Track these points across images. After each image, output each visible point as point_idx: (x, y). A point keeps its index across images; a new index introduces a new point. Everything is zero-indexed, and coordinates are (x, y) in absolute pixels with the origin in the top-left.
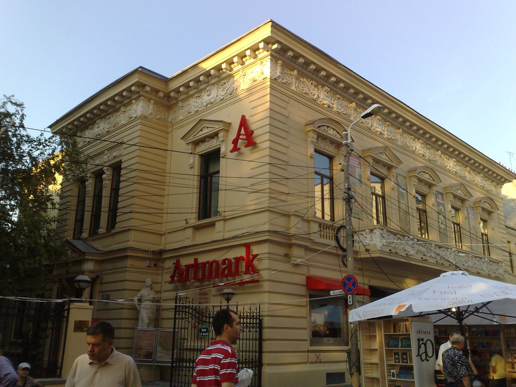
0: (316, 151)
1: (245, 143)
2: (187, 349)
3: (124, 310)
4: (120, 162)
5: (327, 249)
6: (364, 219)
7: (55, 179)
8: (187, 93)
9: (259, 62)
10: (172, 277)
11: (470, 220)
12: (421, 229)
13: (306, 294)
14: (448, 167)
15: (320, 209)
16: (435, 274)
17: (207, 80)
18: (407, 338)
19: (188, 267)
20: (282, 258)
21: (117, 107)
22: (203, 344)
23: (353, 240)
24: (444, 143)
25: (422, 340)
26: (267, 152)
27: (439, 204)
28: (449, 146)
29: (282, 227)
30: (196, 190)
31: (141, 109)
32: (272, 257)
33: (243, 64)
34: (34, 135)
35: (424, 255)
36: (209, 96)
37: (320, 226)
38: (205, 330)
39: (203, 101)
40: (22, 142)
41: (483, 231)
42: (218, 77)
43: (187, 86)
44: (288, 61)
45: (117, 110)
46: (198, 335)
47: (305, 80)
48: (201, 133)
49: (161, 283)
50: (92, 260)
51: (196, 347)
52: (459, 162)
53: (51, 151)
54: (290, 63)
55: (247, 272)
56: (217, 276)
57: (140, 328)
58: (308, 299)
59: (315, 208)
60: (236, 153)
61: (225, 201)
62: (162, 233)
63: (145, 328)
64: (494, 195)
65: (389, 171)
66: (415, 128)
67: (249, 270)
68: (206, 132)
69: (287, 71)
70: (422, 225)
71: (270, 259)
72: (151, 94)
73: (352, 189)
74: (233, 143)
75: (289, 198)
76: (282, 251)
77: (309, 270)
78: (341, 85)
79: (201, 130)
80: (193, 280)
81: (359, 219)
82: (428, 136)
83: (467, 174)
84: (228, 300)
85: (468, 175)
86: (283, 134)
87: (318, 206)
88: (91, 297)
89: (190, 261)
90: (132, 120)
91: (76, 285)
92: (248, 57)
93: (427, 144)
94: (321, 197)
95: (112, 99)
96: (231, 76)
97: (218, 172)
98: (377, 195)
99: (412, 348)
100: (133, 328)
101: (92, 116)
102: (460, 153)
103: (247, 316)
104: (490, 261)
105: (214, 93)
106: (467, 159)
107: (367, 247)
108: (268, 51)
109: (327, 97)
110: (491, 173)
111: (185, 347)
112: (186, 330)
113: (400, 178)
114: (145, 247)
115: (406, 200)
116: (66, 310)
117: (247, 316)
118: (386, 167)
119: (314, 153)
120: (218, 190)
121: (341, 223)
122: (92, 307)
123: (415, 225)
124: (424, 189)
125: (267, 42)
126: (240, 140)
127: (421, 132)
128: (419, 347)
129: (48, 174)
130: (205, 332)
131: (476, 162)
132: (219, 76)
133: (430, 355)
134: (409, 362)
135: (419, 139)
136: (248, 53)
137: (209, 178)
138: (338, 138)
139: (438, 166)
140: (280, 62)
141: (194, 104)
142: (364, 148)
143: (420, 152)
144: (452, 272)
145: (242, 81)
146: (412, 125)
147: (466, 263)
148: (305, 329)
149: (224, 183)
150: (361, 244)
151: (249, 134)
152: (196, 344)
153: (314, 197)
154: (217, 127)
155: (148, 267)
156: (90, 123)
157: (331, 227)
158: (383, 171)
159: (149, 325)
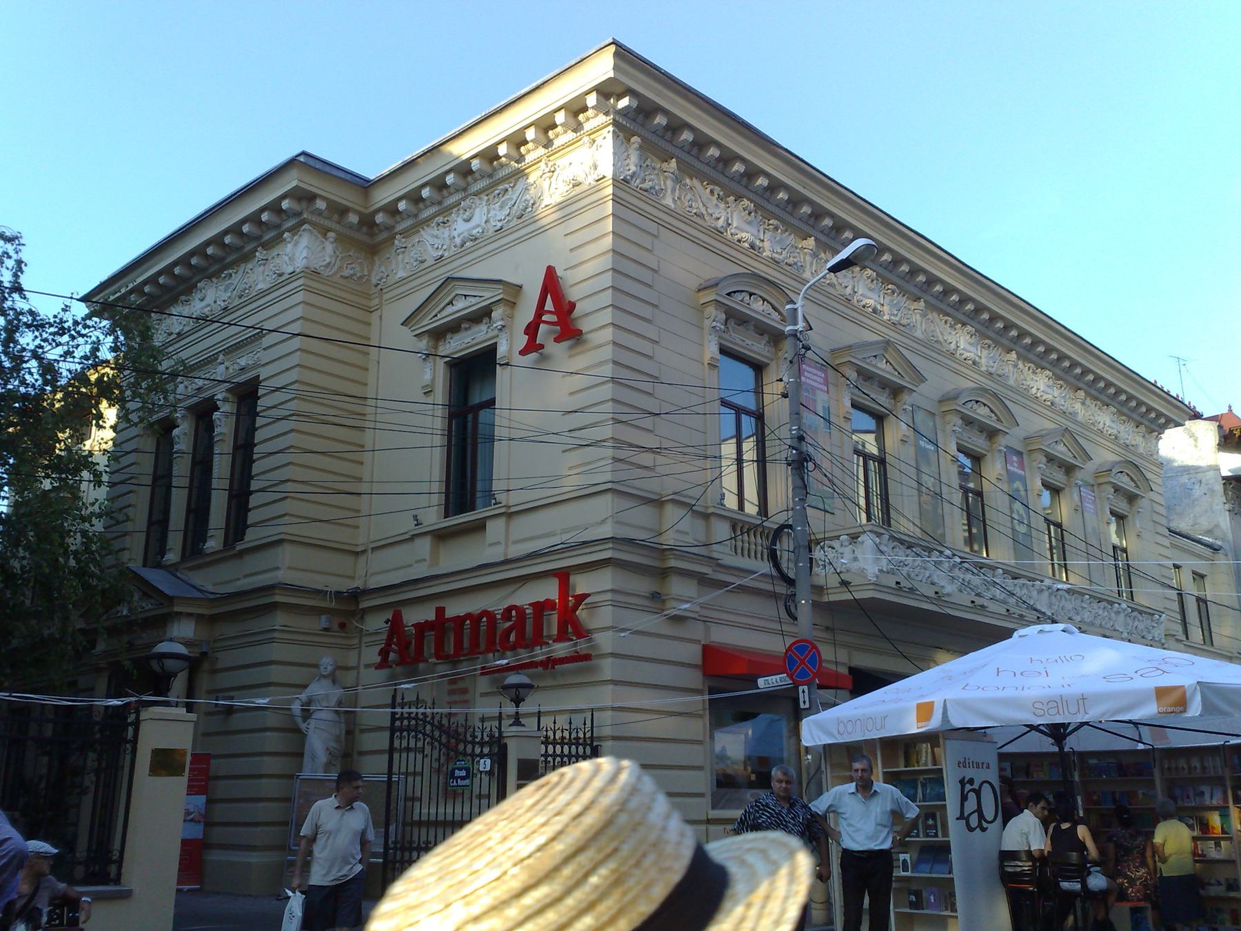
0: (724, 351)
1: (553, 332)
2: (420, 823)
3: (268, 734)
4: (255, 383)
5: (746, 581)
6: (836, 511)
7: (100, 416)
8: (416, 216)
9: (586, 139)
10: (384, 653)
11: (1086, 514)
12: (970, 540)
13: (700, 687)
14: (1034, 390)
15: (734, 484)
16: (1006, 634)
17: (462, 183)
18: (937, 778)
19: (421, 627)
20: (647, 603)
21: (248, 248)
22: (458, 810)
23: (811, 559)
24: (1023, 333)
25: (971, 781)
26: (607, 352)
27: (1012, 477)
28: (1037, 342)
29: (645, 529)
30: (439, 440)
31: (304, 255)
32: (620, 600)
33: (548, 144)
34: (48, 309)
35: (978, 595)
36: (468, 220)
37: (734, 528)
38: (463, 773)
39: (455, 234)
40: (17, 328)
41: (1115, 540)
42: (490, 176)
43: (414, 197)
44: (654, 138)
45: (247, 257)
46: (446, 784)
47: (696, 183)
48: (450, 309)
49: (357, 668)
50: (190, 615)
51: (441, 818)
52: (1058, 378)
53: (88, 347)
54: (662, 143)
55: (562, 637)
56: (491, 648)
57: (306, 773)
58: (707, 697)
59: (722, 487)
60: (533, 356)
61: (511, 467)
62: (359, 549)
63: (320, 775)
64: (1140, 456)
65: (894, 398)
66: (955, 298)
67: (566, 632)
68: (461, 306)
69: (652, 161)
70: (974, 530)
71: (615, 604)
72: (329, 218)
73: (808, 439)
74: (526, 333)
75: (660, 460)
76: (643, 585)
77: (707, 630)
78: (781, 195)
79: (451, 303)
80: (433, 660)
81: (825, 511)
82: (986, 316)
83: (1078, 406)
84: (518, 701)
85: (1082, 409)
86: (646, 311)
87: (730, 482)
88: (190, 693)
89: (427, 614)
90: (283, 280)
91: (155, 665)
92: (559, 129)
93: (983, 336)
94: (735, 456)
95: (235, 229)
96: (520, 174)
97: (491, 403)
98: (867, 457)
99: (948, 802)
100: (291, 777)
101: (186, 273)
102: (1062, 357)
103: (563, 738)
104: (1133, 610)
105: (479, 216)
106: (1078, 371)
107: (845, 577)
108: (607, 114)
109: (749, 223)
110: (1133, 404)
111: (416, 818)
112: (418, 779)
113: (919, 417)
114: (319, 582)
115: (934, 468)
116: (130, 724)
117: (563, 738)
118: (887, 390)
119: (719, 356)
120: (491, 439)
121: (781, 519)
122: (193, 716)
123: (956, 529)
124: (978, 442)
125: (605, 91)
126: (542, 327)
127: (970, 307)
128: (964, 798)
129: (81, 415)
130: (463, 778)
131: (1098, 378)
132: (492, 174)
133: (989, 817)
134: (940, 834)
135: (964, 324)
136: (560, 118)
137: (470, 417)
138: (774, 320)
139: (1011, 388)
140: (635, 139)
141: (432, 241)
142: (836, 346)
143: (966, 355)
144: (1039, 627)
145: (546, 184)
146: (949, 290)
147: (1078, 614)
148: (700, 768)
149: (505, 423)
150: (829, 569)
151: (565, 310)
152: (441, 810)
153: (720, 457)
154: (488, 295)
155: (326, 629)
156: (182, 288)
157: (760, 529)
158: (883, 399)
159: (328, 767)
